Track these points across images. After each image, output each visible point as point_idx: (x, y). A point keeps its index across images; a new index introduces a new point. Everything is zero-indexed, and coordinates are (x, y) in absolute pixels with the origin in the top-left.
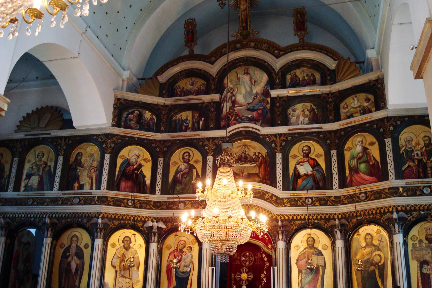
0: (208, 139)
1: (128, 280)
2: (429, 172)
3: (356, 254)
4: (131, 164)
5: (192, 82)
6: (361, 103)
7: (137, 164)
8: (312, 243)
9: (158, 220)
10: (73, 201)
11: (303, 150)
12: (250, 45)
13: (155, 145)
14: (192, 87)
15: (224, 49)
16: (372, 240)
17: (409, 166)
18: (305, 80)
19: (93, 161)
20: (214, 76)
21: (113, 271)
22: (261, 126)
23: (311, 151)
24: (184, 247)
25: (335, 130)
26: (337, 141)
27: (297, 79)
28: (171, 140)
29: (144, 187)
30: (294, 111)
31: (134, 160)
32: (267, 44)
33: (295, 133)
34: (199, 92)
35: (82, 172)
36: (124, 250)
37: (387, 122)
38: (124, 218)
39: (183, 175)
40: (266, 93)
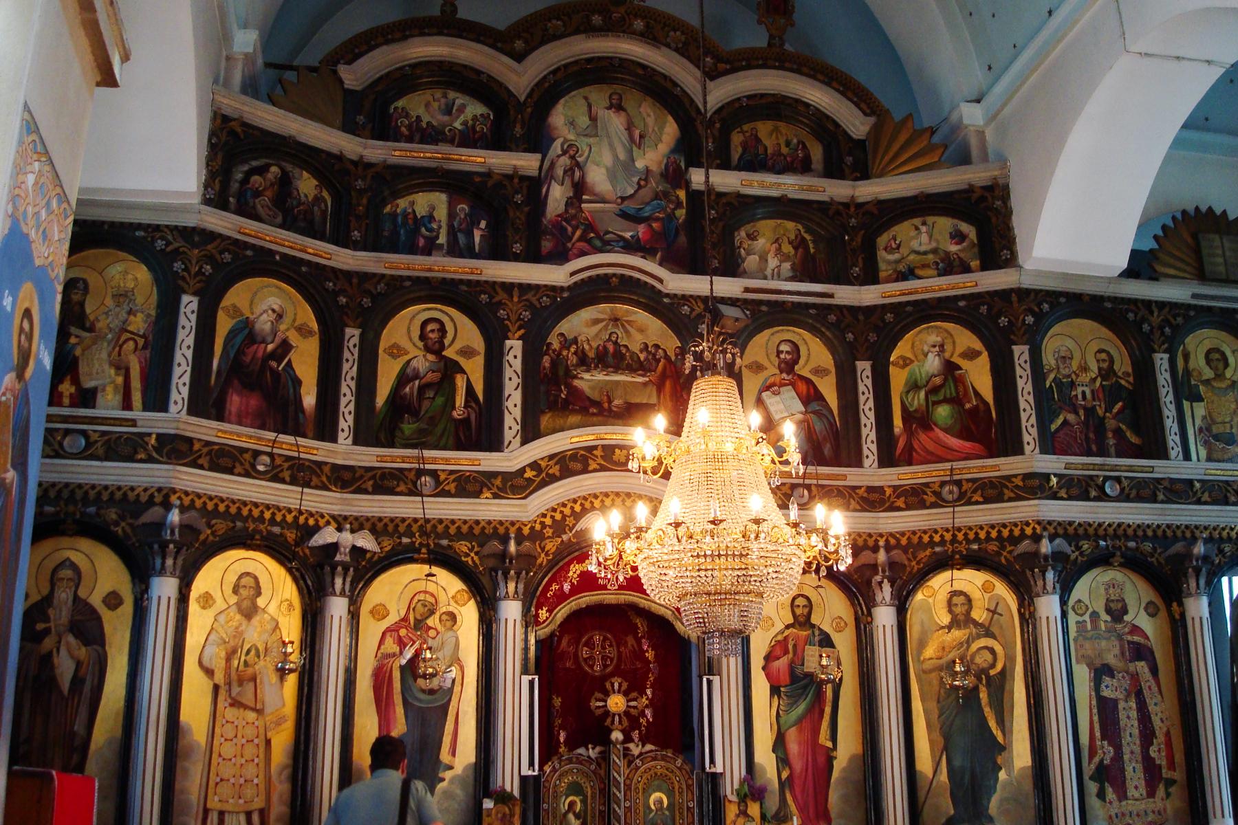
0: (508, 287)
1: (251, 716)
2: (1111, 442)
3: (922, 644)
4: (259, 339)
5: (447, 105)
6: (937, 241)
7: (278, 340)
8: (806, 610)
9: (358, 524)
10: (61, 444)
11: (779, 353)
12: (631, 25)
13: (335, 285)
14: (446, 118)
15: (554, 22)
16: (971, 608)
17: (1065, 422)
18: (780, 154)
19: (130, 312)
20: (522, 99)
21: (207, 685)
22: (660, 264)
23: (799, 357)
24: (432, 612)
25: (867, 307)
26: (872, 337)
27: (761, 150)
28: (383, 276)
29: (296, 418)
30: (752, 237)
31: (268, 327)
32: (683, 33)
33: (761, 302)
34: (469, 139)
35: (88, 347)
36: (238, 617)
37: (1019, 301)
38: (245, 512)
39: (422, 389)
40: (674, 176)
